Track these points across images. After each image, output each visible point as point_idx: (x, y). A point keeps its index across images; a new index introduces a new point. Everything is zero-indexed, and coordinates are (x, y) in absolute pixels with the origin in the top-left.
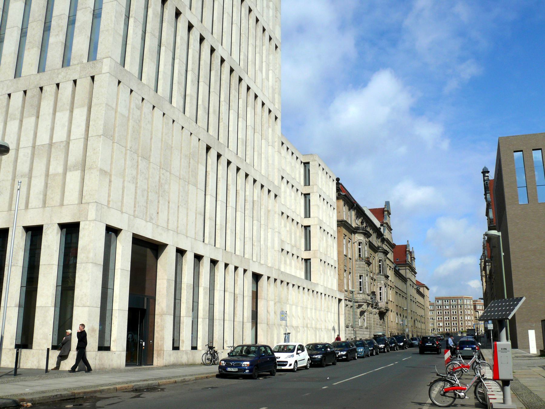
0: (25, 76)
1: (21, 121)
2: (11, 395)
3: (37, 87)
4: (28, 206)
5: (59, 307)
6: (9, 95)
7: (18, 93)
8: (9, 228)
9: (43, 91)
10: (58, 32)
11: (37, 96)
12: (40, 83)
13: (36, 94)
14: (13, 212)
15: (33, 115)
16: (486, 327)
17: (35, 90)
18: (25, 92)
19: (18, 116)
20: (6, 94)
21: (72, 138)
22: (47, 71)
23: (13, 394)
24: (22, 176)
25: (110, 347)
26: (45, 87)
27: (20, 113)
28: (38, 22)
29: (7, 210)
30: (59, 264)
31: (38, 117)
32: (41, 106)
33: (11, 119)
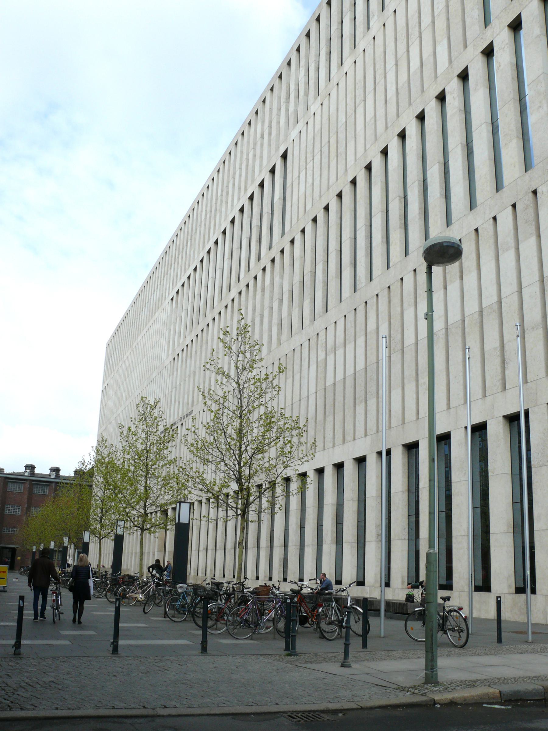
0: (509, 184)
1: (518, 249)
2: (534, 677)
3: (529, 193)
4: (505, 388)
5: (445, 537)
6: (495, 218)
7: (505, 211)
8: (486, 421)
9: (538, 194)
10: (540, 102)
11: (532, 205)
12: (531, 186)
13: (529, 203)
14: (380, 433)
15: (531, 234)
16: (417, 549)
17: (527, 197)
18: (514, 206)
19: (511, 242)
20: (490, 219)
21: (419, 339)
22: (538, 164)
23: (538, 675)
24: (533, 328)
25: (341, 581)
26: (540, 187)
27: (513, 238)
28: (510, 103)
29: (400, 424)
30: (514, 473)
31: (539, 236)
32: (540, 218)
33: (503, 251)
